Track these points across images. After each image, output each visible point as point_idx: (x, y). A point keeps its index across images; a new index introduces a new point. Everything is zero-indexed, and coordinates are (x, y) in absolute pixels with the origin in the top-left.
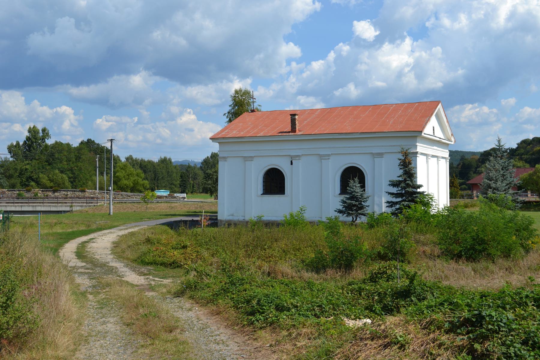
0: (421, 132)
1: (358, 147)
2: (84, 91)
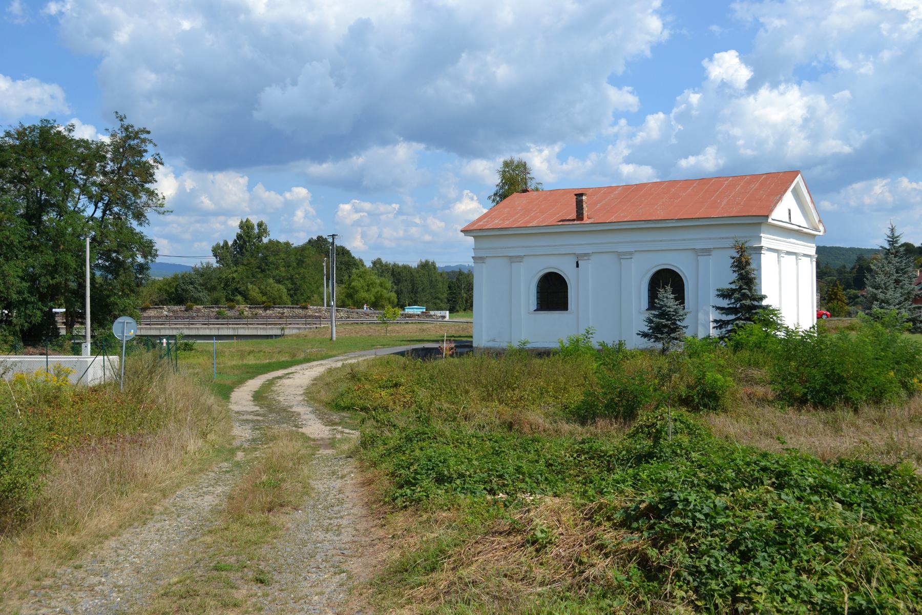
0: (767, 217)
1: (674, 240)
2: (325, 169)
